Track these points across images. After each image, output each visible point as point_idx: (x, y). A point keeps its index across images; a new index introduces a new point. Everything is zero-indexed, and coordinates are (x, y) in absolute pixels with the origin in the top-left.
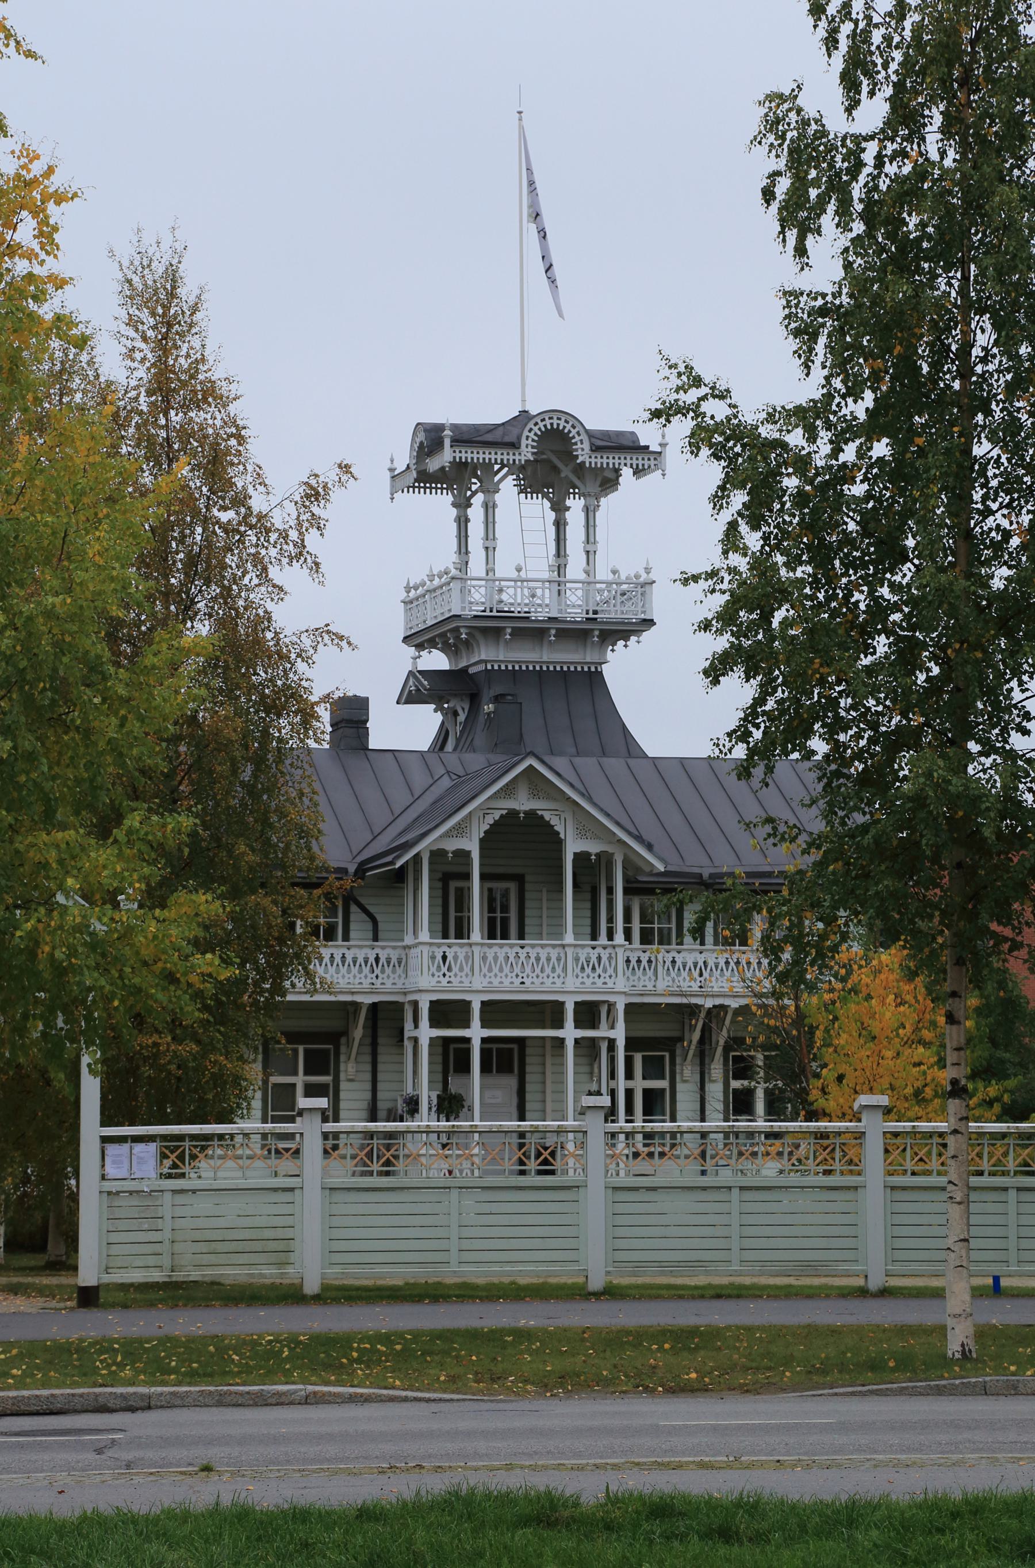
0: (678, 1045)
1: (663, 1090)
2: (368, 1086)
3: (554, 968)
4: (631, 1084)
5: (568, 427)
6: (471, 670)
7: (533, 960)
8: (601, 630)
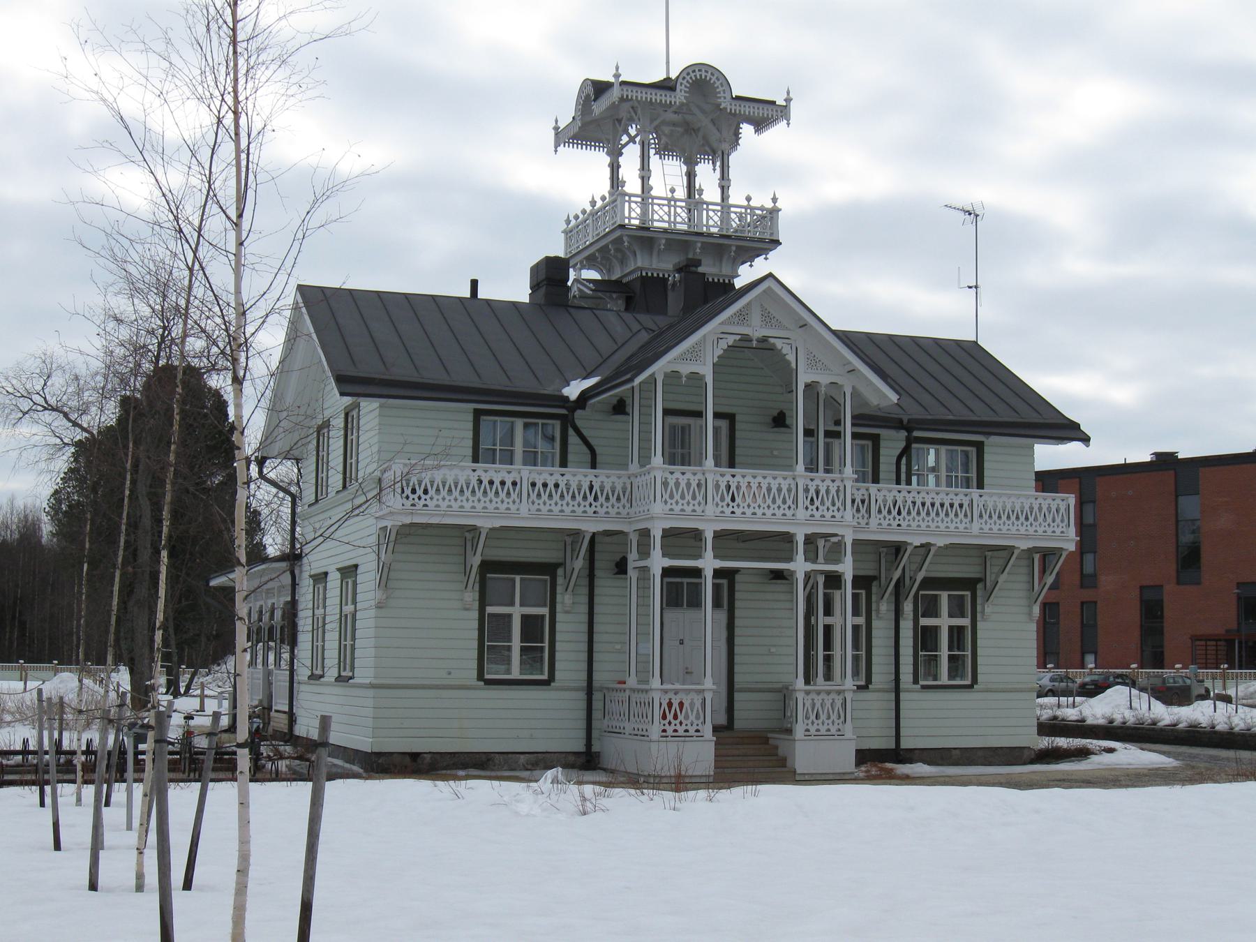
0: (875, 583)
1: (543, 617)
2: (585, 618)
3: (774, 498)
4: (829, 620)
5: (714, 79)
6: (624, 281)
7: (764, 490)
8: (738, 247)
